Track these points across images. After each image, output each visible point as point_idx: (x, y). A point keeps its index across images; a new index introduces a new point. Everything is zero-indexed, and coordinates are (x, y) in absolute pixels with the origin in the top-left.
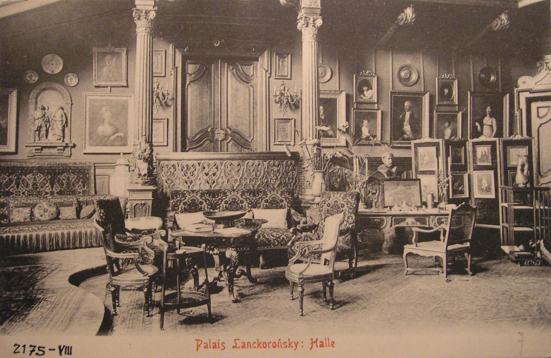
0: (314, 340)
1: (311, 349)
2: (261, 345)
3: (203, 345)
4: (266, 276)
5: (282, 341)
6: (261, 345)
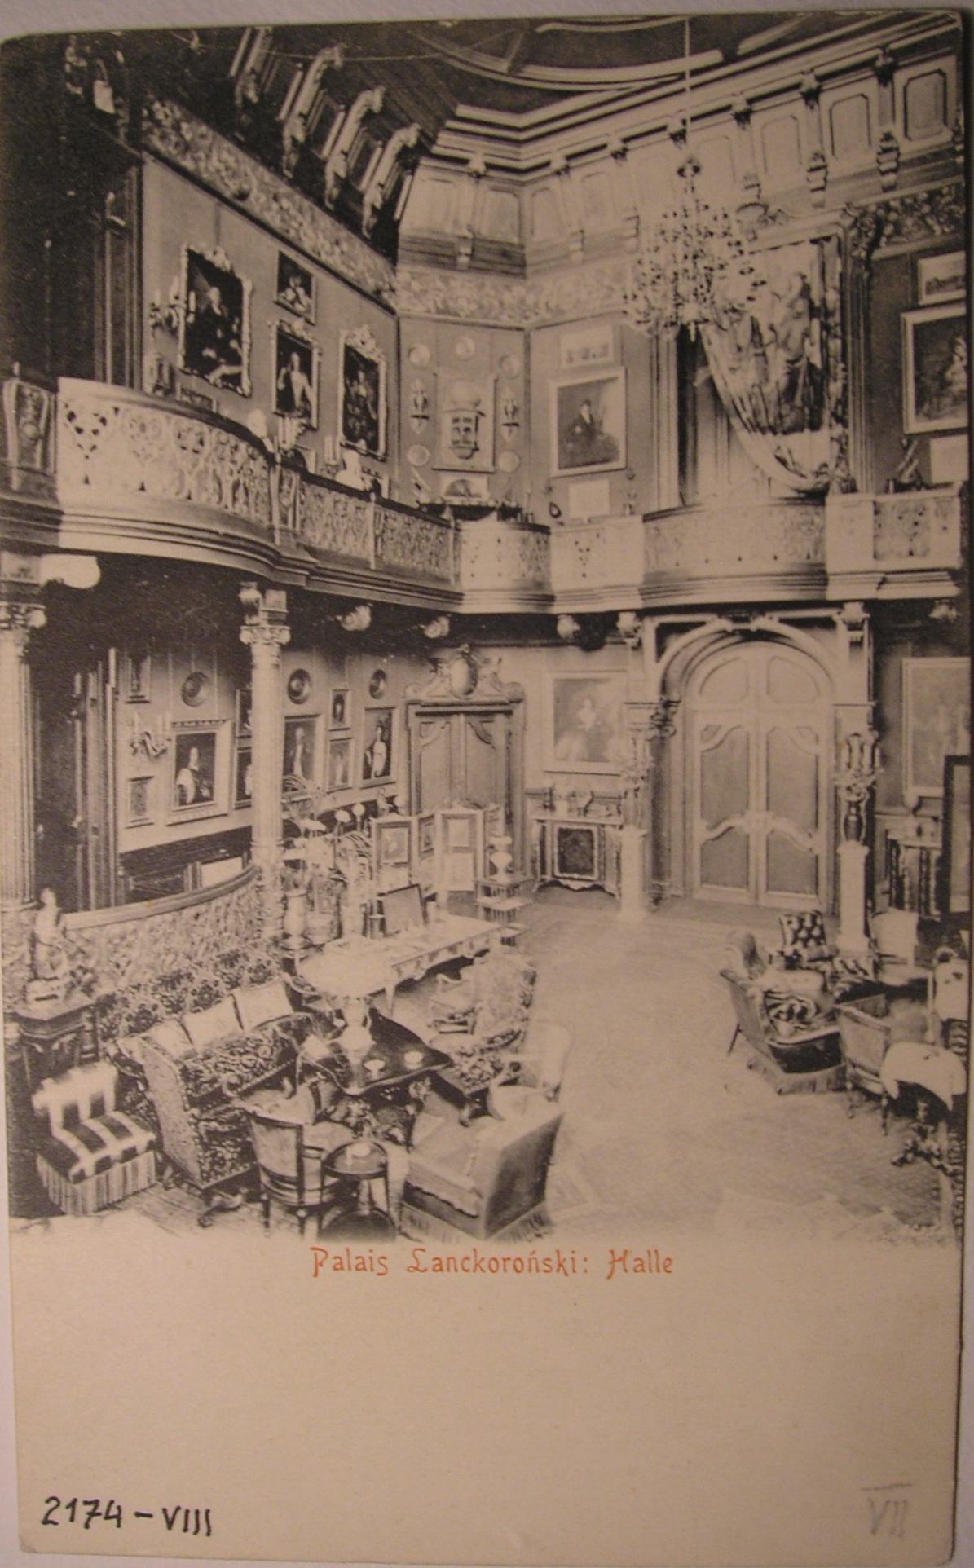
0: (619, 1254)
1: (609, 1277)
2: (484, 1265)
3: (330, 1262)
4: (34, 700)
5: (540, 1256)
6: (484, 1265)
